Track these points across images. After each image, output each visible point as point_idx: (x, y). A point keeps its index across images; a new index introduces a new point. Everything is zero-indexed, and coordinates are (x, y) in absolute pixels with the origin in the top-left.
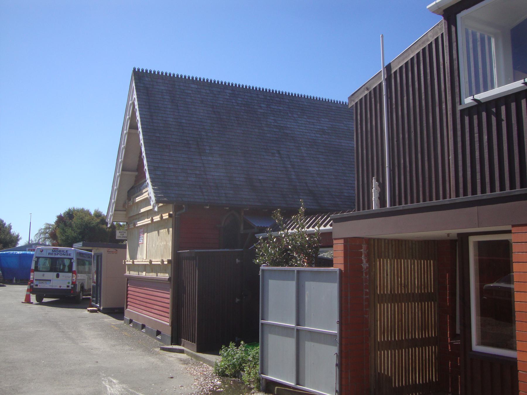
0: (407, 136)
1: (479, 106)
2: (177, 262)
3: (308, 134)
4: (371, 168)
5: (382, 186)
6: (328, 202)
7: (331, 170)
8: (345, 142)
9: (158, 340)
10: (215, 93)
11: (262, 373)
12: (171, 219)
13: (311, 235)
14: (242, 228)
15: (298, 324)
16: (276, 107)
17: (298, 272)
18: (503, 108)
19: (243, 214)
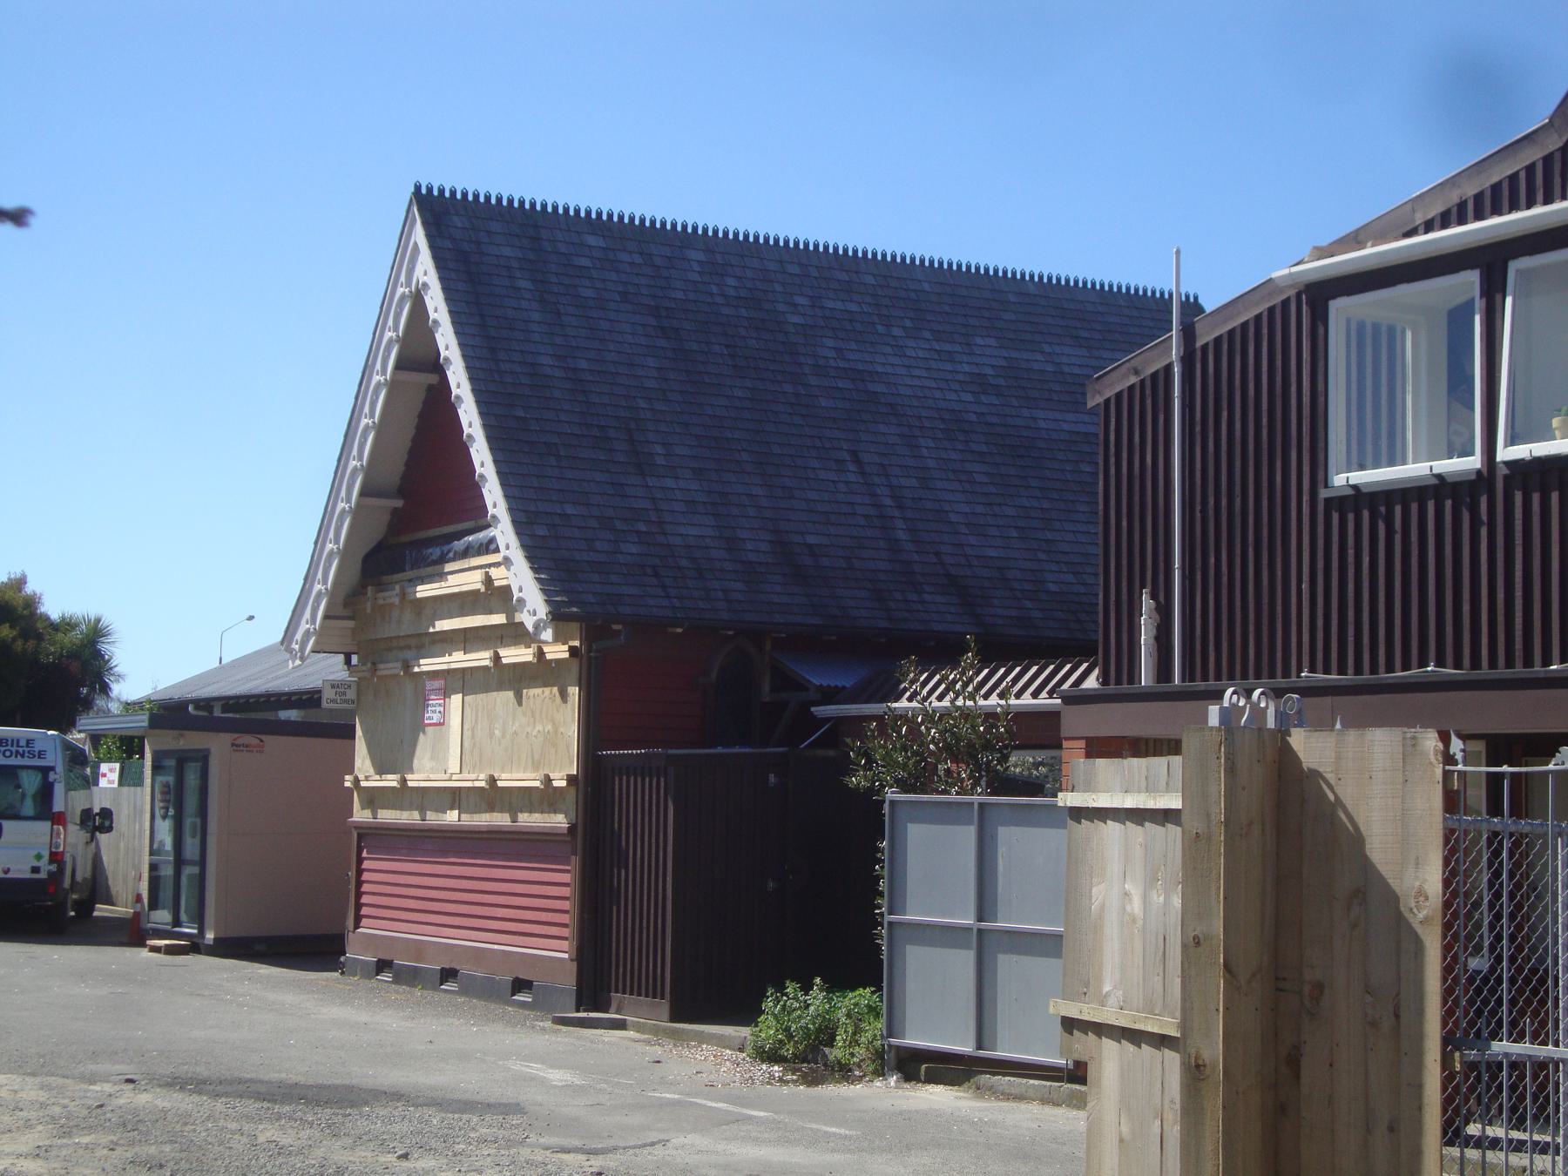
0: (1224, 502)
1: (1359, 498)
2: (595, 780)
3: (938, 395)
4: (1140, 564)
5: (1164, 611)
6: (1000, 611)
7: (1010, 511)
8: (1051, 415)
9: (523, 1005)
10: (658, 261)
11: (890, 1035)
12: (576, 662)
13: (991, 716)
14: (767, 688)
15: (980, 919)
16: (839, 305)
17: (982, 805)
18: (1398, 509)
19: (768, 647)
